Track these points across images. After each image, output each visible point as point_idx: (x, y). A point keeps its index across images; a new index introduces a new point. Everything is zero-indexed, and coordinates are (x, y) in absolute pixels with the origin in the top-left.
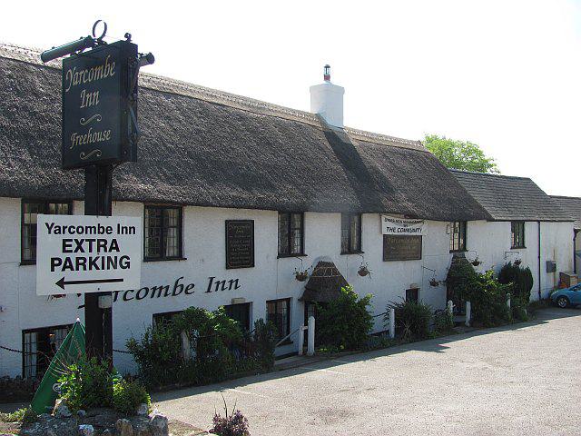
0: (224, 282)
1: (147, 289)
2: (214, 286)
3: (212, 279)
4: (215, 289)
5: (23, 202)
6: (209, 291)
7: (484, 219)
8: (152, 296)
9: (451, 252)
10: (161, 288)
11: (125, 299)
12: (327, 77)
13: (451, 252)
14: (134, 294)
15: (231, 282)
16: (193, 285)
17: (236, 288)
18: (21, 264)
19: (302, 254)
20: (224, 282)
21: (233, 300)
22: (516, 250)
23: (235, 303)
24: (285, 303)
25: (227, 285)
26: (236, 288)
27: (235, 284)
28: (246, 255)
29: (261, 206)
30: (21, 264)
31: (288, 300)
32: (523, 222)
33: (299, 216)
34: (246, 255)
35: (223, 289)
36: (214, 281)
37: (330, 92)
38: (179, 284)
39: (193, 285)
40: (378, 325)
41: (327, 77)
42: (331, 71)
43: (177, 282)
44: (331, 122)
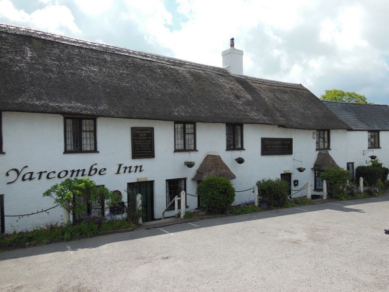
0: (131, 167)
1: (67, 172)
2: (122, 170)
3: (120, 165)
4: (134, 171)
5: (65, 119)
6: (118, 173)
7: (345, 129)
8: (125, 172)
9: (317, 150)
10: (79, 171)
11: (48, 177)
12: (232, 45)
13: (317, 150)
14: (56, 175)
15: (137, 167)
16: (105, 169)
17: (140, 171)
18: (64, 153)
19: (195, 150)
20: (131, 167)
21: (138, 179)
22: (371, 150)
23: (139, 181)
24: (183, 181)
25: (133, 169)
26: (140, 171)
27: (140, 169)
28: (148, 150)
29: (301, 127)
30: (64, 153)
31: (185, 179)
32: (378, 131)
33: (192, 126)
34: (148, 150)
35: (130, 172)
36: (122, 167)
37: (233, 52)
38: (93, 168)
39: (105, 169)
40: (239, 199)
41: (232, 45)
42: (235, 41)
43: (92, 167)
44: (234, 72)
